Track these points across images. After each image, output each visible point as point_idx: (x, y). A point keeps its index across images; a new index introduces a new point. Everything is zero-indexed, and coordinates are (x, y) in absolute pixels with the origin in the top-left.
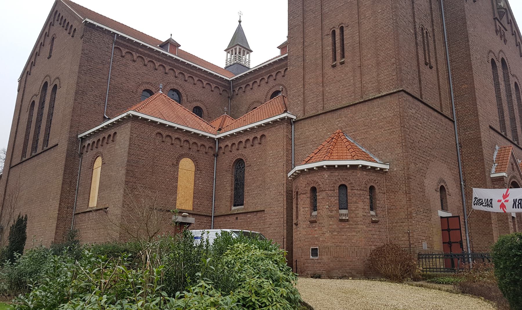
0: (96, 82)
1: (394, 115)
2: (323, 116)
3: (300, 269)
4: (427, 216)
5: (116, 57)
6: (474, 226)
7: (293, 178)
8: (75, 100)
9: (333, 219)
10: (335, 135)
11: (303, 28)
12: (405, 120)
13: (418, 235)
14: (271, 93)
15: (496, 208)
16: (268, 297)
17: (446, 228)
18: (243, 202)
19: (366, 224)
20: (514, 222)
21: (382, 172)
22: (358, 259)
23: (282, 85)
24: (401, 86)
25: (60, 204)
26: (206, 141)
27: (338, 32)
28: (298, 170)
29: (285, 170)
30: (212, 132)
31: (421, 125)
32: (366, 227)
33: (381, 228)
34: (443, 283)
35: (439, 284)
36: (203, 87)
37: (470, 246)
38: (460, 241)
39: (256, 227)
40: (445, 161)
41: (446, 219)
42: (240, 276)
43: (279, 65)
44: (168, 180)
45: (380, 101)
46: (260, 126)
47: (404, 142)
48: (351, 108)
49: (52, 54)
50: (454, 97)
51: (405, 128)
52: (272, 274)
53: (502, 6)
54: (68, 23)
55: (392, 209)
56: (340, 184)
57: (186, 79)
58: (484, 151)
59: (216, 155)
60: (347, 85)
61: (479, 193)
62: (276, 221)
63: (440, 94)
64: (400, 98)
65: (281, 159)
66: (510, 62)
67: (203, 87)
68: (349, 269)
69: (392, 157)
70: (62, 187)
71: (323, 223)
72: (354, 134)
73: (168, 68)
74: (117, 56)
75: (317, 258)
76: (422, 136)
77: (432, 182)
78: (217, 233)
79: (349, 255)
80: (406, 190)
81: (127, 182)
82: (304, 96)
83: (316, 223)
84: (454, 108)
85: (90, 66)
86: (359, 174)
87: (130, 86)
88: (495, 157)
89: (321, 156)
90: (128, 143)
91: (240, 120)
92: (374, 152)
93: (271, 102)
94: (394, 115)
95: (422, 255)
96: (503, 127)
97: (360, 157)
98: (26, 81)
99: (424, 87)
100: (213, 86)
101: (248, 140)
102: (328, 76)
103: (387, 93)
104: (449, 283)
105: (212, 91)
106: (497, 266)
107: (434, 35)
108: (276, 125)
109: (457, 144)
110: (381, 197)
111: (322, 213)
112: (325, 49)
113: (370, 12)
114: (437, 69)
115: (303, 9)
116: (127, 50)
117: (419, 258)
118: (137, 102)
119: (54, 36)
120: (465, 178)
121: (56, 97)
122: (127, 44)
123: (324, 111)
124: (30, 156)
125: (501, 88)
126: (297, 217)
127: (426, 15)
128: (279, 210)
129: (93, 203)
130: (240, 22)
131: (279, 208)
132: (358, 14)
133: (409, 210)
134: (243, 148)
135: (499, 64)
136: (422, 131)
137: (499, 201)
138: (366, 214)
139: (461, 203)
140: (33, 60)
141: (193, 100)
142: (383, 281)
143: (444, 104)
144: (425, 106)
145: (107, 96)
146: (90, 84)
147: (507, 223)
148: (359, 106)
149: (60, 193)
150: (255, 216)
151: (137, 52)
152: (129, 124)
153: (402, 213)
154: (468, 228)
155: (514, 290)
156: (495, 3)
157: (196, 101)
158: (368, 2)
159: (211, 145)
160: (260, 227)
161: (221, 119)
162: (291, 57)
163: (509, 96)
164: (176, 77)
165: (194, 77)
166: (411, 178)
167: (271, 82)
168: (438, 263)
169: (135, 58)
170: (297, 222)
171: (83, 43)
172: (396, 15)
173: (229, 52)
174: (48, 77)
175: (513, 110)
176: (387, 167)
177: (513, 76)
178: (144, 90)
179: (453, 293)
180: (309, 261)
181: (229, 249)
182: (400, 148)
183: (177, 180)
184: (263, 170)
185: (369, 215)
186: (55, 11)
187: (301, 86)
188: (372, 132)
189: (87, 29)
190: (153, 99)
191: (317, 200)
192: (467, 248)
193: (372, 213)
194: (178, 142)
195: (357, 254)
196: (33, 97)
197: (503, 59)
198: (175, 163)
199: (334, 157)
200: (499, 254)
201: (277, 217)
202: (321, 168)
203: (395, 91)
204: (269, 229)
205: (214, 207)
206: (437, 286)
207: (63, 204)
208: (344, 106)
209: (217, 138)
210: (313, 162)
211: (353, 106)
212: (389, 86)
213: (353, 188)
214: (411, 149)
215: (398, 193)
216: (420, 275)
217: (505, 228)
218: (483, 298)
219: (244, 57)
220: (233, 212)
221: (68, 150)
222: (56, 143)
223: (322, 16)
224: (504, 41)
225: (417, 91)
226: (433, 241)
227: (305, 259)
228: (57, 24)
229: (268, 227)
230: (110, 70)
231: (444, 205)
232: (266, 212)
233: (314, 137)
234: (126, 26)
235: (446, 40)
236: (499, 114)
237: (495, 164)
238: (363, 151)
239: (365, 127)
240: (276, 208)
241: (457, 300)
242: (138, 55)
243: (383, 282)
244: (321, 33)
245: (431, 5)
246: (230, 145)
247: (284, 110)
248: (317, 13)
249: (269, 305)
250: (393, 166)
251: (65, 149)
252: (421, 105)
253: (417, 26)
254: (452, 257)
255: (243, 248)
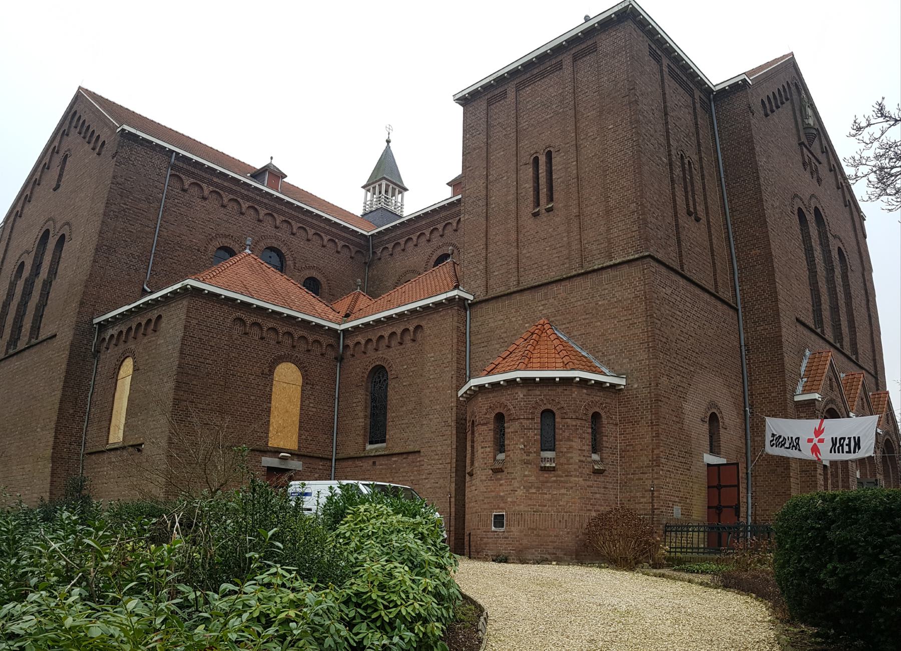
0: (135, 231)
1: (636, 297)
2: (518, 297)
3: (475, 546)
4: (685, 463)
5: (172, 190)
6: (762, 481)
7: (466, 398)
8: (94, 261)
9: (530, 466)
10: (536, 328)
11: (487, 153)
12: (654, 304)
13: (667, 495)
14: (435, 258)
15: (806, 453)
16: (401, 593)
17: (716, 484)
18: (385, 437)
19: (584, 476)
20: (825, 474)
21: (614, 391)
22: (568, 533)
23: (453, 245)
24: (647, 249)
25: (56, 437)
26: (322, 334)
27: (543, 159)
28: (474, 386)
29: (454, 386)
30: (334, 319)
31: (681, 314)
32: (584, 480)
33: (607, 482)
34: (698, 572)
35: (691, 573)
36: (324, 246)
37: (752, 513)
38: (736, 504)
39: (406, 478)
40: (721, 373)
41: (716, 468)
42: (356, 559)
43: (449, 213)
44: (252, 398)
45: (611, 273)
46: (413, 311)
47: (651, 342)
48: (563, 283)
49: (61, 183)
50: (738, 270)
51: (653, 317)
52: (412, 556)
53: (810, 125)
54: (93, 131)
55: (628, 451)
56: (543, 408)
57: (295, 231)
58: (786, 359)
59: (340, 359)
60: (558, 246)
61: (776, 426)
62: (439, 469)
63: (714, 264)
64: (646, 269)
65: (448, 367)
66: (827, 214)
67: (324, 246)
68: (552, 547)
69: (630, 366)
70: (60, 409)
71: (513, 473)
72: (568, 328)
73: (263, 212)
74: (174, 190)
75: (502, 530)
76: (682, 332)
77: (696, 408)
78: (331, 486)
79: (554, 525)
80: (651, 420)
81: (177, 399)
82: (486, 263)
83: (502, 473)
84: (738, 288)
85: (125, 204)
86: (576, 393)
87: (194, 240)
88: (803, 369)
89: (513, 363)
90: (180, 334)
91: (382, 300)
92: (601, 356)
93: (434, 272)
94: (636, 297)
95: (671, 526)
96: (819, 320)
97: (577, 366)
98: (12, 229)
99: (686, 252)
100: (340, 244)
101: (393, 334)
102: (526, 230)
103: (624, 259)
104: (708, 572)
105: (338, 252)
106: (781, 544)
107: (702, 168)
108: (440, 310)
109: (741, 346)
110: (610, 431)
111: (513, 456)
112: (522, 187)
113: (595, 129)
114: (708, 222)
115: (487, 122)
116: (193, 180)
117: (666, 531)
118: (206, 267)
119: (68, 153)
120: (753, 402)
121: (63, 255)
122: (193, 170)
123: (519, 288)
124: (5, 354)
125: (815, 256)
126: (472, 463)
127: (688, 135)
128: (444, 450)
129: (117, 436)
130: (388, 142)
131: (445, 447)
132: (576, 130)
133: (656, 452)
134: (385, 347)
135: (810, 218)
136: (681, 324)
137: (810, 441)
138: (584, 459)
139: (744, 441)
140: (29, 193)
141: (304, 266)
142: (603, 568)
143: (721, 281)
144: (688, 283)
145: (152, 255)
146: (124, 235)
147: (814, 476)
148: (577, 281)
149: (55, 418)
150: (404, 460)
151: (211, 183)
152: (184, 302)
153: (644, 458)
154: (752, 484)
155: (799, 585)
156: (799, 120)
157: (310, 268)
158: (592, 113)
159: (332, 341)
160: (412, 478)
161: (350, 298)
162: (467, 199)
163: (830, 270)
164: (276, 227)
165: (307, 228)
166: (660, 401)
167: (436, 240)
168: (695, 540)
169: (206, 193)
170: (472, 470)
171: (116, 165)
172: (638, 133)
173: (369, 190)
174: (51, 222)
175: (836, 294)
176: (622, 382)
177: (835, 237)
178: (219, 248)
179: (710, 587)
180: (490, 535)
181: (350, 514)
182: (644, 351)
183: (270, 399)
184: (418, 385)
185: (589, 459)
186: (73, 111)
187: (482, 247)
188: (599, 324)
189: (124, 141)
190: (234, 262)
191: (506, 435)
192: (747, 516)
193: (595, 457)
194: (272, 335)
195: (566, 525)
196: (22, 254)
197: (816, 209)
198: (266, 371)
199: (535, 365)
200: (787, 527)
201: (441, 462)
202: (511, 383)
203: (637, 256)
204: (427, 481)
205: (336, 446)
206: (687, 576)
207: (61, 437)
208: (552, 280)
209: (341, 330)
210: (499, 373)
211: (568, 281)
212: (626, 249)
213: (564, 415)
214: (662, 352)
215: (638, 424)
216: (665, 558)
217: (811, 484)
218: (754, 595)
219: (394, 198)
220: (368, 453)
221: (72, 345)
222: (54, 332)
223: (517, 133)
224: (818, 180)
225: (674, 259)
226: (692, 504)
227: (484, 532)
228: (74, 132)
229: (425, 479)
230: (161, 212)
231: (715, 444)
232: (422, 454)
233: (502, 331)
234: (194, 140)
235: (722, 176)
236: (812, 299)
237: (803, 379)
238: (583, 356)
239: (588, 316)
240: (439, 448)
241: (714, 597)
242: (211, 188)
243: (603, 570)
244: (515, 161)
245: (696, 118)
246: (363, 342)
247: (455, 285)
248: (509, 129)
249: (402, 604)
250: (632, 381)
251: (68, 343)
252: (682, 282)
253: (673, 152)
254: (719, 529)
255: (375, 512)
